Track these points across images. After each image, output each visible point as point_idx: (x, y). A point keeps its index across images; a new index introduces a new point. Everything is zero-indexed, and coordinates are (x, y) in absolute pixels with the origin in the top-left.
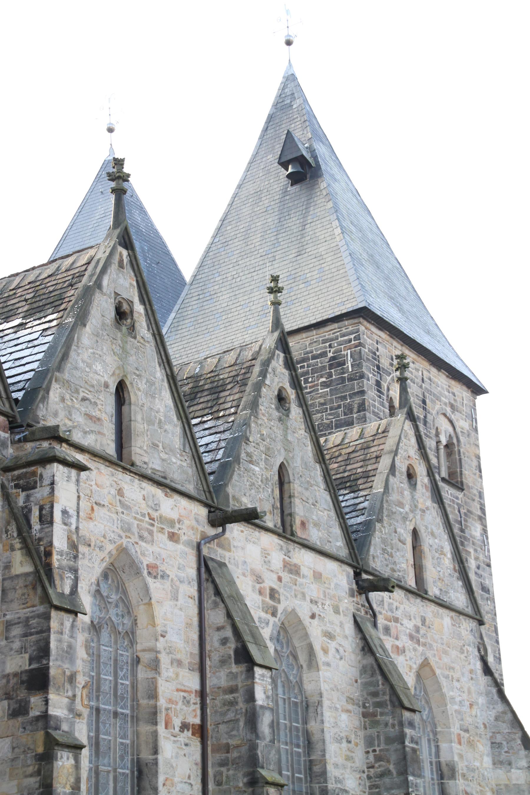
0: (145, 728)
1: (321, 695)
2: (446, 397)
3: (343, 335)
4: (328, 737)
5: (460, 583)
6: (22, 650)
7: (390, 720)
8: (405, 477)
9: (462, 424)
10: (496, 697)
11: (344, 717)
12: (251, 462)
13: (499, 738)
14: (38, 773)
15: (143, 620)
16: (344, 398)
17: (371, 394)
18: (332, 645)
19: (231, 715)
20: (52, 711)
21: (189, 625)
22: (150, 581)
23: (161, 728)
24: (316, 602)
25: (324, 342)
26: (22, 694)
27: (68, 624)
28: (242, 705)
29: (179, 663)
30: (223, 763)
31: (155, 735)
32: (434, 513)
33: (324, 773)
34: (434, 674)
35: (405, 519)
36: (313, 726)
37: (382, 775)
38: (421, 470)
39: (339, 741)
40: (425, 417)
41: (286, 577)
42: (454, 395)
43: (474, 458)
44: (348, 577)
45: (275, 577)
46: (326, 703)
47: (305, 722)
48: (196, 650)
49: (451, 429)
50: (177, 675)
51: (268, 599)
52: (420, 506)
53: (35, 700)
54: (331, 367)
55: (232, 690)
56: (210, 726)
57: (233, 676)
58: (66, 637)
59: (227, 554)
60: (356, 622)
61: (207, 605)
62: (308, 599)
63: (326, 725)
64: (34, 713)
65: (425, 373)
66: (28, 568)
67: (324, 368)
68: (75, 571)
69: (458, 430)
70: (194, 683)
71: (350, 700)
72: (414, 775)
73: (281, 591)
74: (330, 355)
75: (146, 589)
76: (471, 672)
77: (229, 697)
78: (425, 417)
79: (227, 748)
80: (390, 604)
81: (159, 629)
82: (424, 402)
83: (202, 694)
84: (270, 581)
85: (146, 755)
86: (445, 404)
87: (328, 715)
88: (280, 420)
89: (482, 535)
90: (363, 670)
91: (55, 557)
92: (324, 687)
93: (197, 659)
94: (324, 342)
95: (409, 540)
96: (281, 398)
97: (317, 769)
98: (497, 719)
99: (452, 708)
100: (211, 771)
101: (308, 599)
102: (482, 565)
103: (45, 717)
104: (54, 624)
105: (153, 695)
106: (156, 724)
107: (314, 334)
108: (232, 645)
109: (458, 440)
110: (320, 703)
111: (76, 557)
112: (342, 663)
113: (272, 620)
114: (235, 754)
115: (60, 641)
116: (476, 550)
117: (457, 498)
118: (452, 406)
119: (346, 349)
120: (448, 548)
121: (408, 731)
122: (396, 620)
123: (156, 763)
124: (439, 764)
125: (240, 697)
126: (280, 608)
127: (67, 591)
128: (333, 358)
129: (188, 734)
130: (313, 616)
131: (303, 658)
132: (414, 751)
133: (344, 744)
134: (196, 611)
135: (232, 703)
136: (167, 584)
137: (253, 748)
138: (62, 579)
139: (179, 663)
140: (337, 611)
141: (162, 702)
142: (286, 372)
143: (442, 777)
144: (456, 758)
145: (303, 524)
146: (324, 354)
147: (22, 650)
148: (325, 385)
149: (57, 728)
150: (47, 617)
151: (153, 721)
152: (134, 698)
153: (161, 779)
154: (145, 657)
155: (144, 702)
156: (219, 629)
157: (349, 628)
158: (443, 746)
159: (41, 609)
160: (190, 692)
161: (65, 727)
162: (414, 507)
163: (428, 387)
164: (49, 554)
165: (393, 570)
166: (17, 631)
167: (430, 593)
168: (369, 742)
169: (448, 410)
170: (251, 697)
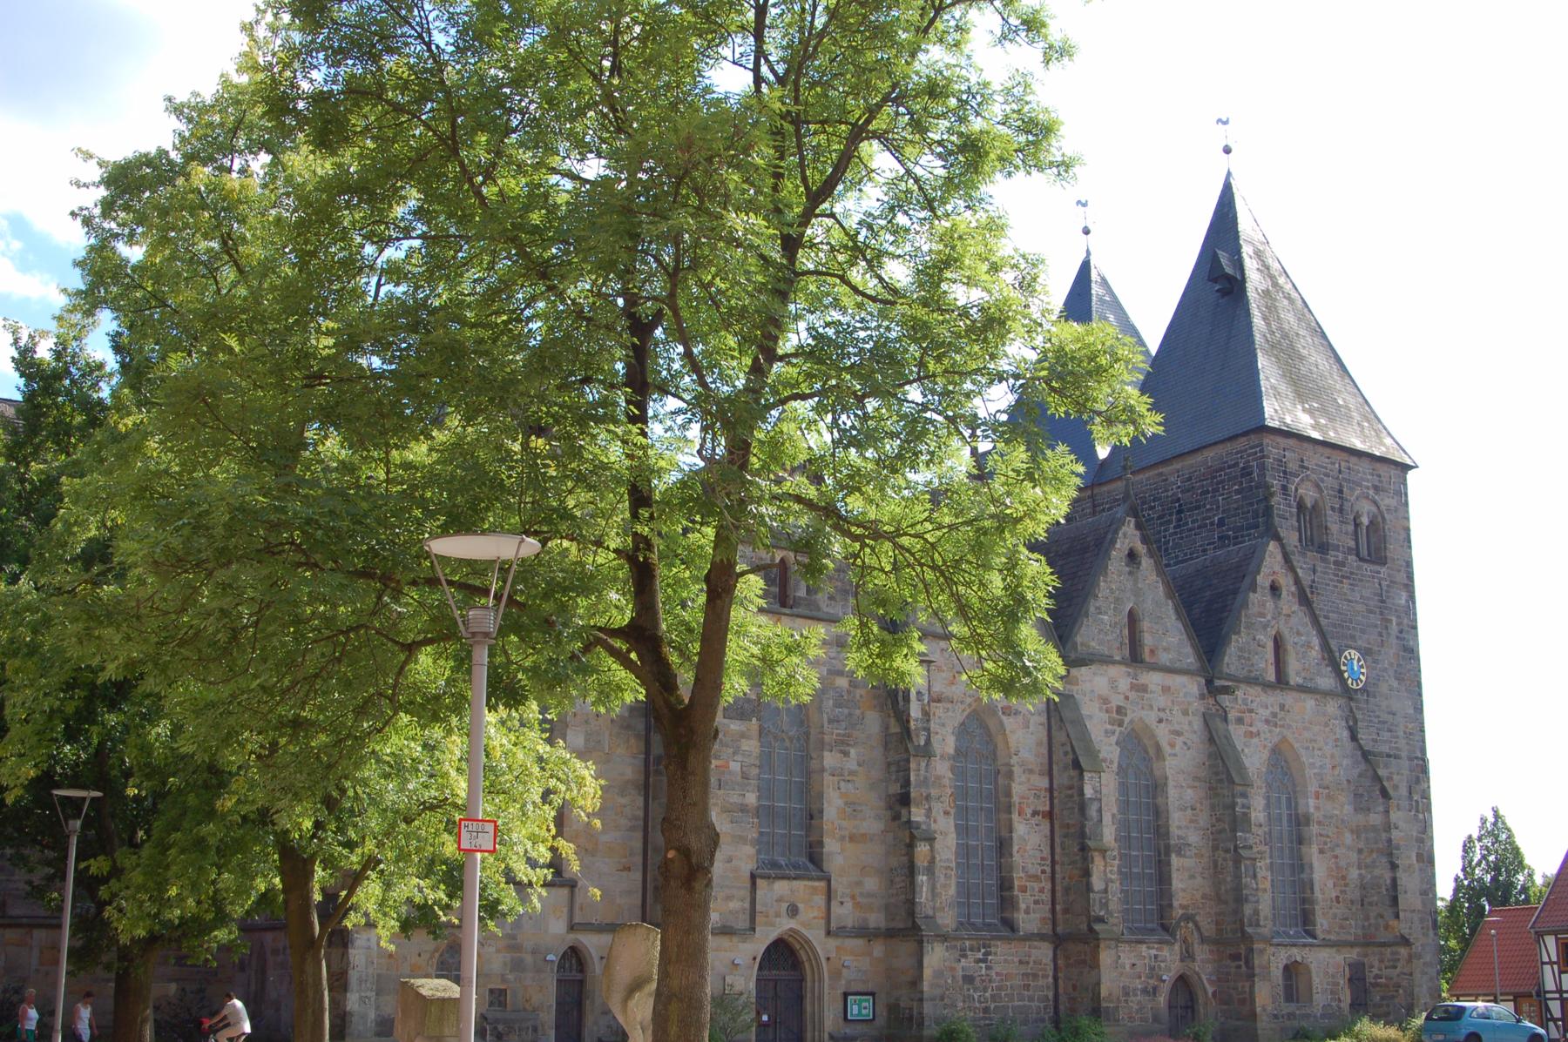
0: (1003, 816)
1: (1166, 778)
2: (1368, 481)
3: (1251, 448)
4: (1171, 808)
5: (1330, 669)
6: (897, 780)
7: (1226, 792)
8: (1267, 591)
9: (1387, 501)
10: (1360, 758)
11: (1189, 791)
12: (1100, 613)
13: (1361, 791)
14: (907, 854)
15: (1000, 745)
16: (1252, 504)
17: (1278, 503)
18: (1179, 741)
19: (1070, 805)
20: (913, 819)
21: (1039, 744)
22: (1004, 718)
23: (1015, 817)
24: (1164, 710)
25: (1237, 453)
26: (897, 807)
27: (923, 764)
28: (1076, 798)
29: (1031, 771)
30: (1066, 836)
31: (1010, 821)
32: (1301, 614)
33: (1168, 833)
34: (1292, 747)
35: (1265, 627)
36: (1160, 800)
37: (1220, 832)
38: (1286, 582)
39: (1183, 809)
40: (1341, 506)
41: (1133, 695)
42: (1379, 476)
43: (1402, 532)
44: (1199, 685)
45: (1122, 697)
46: (1171, 783)
47: (1154, 797)
48: (1046, 761)
49: (1374, 509)
50: (1029, 780)
51: (1114, 715)
52: (1284, 612)
53: (904, 812)
54: (1242, 476)
55: (1071, 788)
56: (1056, 810)
57: (1071, 778)
58: (922, 772)
59: (1075, 688)
60: (1205, 720)
61: (1054, 728)
62: (1156, 708)
63: (1170, 799)
64: (904, 819)
65: (1343, 464)
66: (897, 730)
67: (1236, 477)
68: (928, 730)
69: (1383, 508)
70: (1045, 783)
71: (1196, 778)
72: (1242, 831)
73: (1128, 706)
74: (1241, 465)
75: (1001, 723)
76: (1337, 740)
77: (1070, 792)
78: (1341, 506)
79: (1068, 826)
80: (1244, 700)
81: (1012, 750)
82: (1341, 491)
83: (1051, 790)
84: (1117, 700)
85: (1004, 833)
86: (1368, 488)
87: (1172, 792)
88: (1130, 573)
89: (1407, 601)
90: (1210, 756)
91: (912, 723)
92: (1169, 772)
93: (1047, 767)
94: (1237, 453)
95: (1270, 645)
96: (1132, 556)
97: (1162, 830)
98: (1360, 776)
99: (1309, 773)
100: (1057, 840)
101: (1156, 708)
102: (1406, 628)
103: (909, 821)
104: (913, 765)
105: (1009, 794)
106: (1010, 813)
107: (1229, 446)
108: (1070, 756)
109: (1383, 518)
110: (1166, 784)
111: (928, 721)
112: (1188, 752)
113: (1118, 729)
114: (1072, 830)
115: (918, 775)
116: (1398, 617)
117: (1379, 573)
118: (1376, 488)
119: (1254, 460)
120: (1316, 642)
121: (1239, 800)
122: (1251, 711)
123: (1011, 838)
124: (1297, 815)
125: (1074, 792)
126: (1127, 720)
127: (922, 743)
128: (1243, 468)
129: (1038, 818)
130: (1160, 721)
131: (1152, 752)
132: (1245, 814)
133: (1189, 811)
134: (1045, 733)
135: (1072, 796)
136: (1020, 718)
137: (1083, 827)
138: (918, 736)
139: (1031, 771)
140: (1185, 713)
141: (1016, 799)
142: (1138, 533)
143: (1299, 824)
144: (1312, 810)
145: (1152, 652)
146: (1236, 464)
147: (897, 780)
148: (1238, 492)
149: (918, 828)
150: (908, 761)
151: (1009, 810)
152: (997, 797)
153: (1015, 848)
154: (1003, 769)
155: (1003, 799)
156: (1063, 745)
157: (1197, 723)
158: (1301, 802)
159: (904, 756)
160: (1040, 790)
161: (924, 827)
162: (1278, 614)
163: (1347, 476)
164: (908, 721)
165: (1250, 671)
166: (893, 768)
167: (1292, 683)
168: (1213, 807)
169: (1371, 492)
170: (1081, 793)
